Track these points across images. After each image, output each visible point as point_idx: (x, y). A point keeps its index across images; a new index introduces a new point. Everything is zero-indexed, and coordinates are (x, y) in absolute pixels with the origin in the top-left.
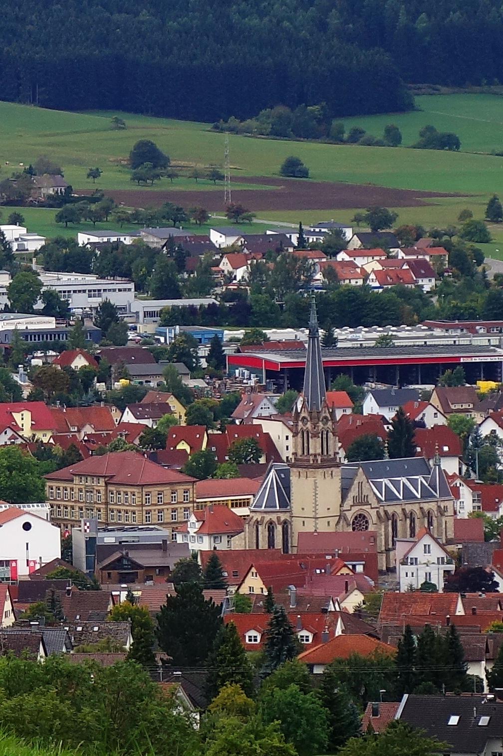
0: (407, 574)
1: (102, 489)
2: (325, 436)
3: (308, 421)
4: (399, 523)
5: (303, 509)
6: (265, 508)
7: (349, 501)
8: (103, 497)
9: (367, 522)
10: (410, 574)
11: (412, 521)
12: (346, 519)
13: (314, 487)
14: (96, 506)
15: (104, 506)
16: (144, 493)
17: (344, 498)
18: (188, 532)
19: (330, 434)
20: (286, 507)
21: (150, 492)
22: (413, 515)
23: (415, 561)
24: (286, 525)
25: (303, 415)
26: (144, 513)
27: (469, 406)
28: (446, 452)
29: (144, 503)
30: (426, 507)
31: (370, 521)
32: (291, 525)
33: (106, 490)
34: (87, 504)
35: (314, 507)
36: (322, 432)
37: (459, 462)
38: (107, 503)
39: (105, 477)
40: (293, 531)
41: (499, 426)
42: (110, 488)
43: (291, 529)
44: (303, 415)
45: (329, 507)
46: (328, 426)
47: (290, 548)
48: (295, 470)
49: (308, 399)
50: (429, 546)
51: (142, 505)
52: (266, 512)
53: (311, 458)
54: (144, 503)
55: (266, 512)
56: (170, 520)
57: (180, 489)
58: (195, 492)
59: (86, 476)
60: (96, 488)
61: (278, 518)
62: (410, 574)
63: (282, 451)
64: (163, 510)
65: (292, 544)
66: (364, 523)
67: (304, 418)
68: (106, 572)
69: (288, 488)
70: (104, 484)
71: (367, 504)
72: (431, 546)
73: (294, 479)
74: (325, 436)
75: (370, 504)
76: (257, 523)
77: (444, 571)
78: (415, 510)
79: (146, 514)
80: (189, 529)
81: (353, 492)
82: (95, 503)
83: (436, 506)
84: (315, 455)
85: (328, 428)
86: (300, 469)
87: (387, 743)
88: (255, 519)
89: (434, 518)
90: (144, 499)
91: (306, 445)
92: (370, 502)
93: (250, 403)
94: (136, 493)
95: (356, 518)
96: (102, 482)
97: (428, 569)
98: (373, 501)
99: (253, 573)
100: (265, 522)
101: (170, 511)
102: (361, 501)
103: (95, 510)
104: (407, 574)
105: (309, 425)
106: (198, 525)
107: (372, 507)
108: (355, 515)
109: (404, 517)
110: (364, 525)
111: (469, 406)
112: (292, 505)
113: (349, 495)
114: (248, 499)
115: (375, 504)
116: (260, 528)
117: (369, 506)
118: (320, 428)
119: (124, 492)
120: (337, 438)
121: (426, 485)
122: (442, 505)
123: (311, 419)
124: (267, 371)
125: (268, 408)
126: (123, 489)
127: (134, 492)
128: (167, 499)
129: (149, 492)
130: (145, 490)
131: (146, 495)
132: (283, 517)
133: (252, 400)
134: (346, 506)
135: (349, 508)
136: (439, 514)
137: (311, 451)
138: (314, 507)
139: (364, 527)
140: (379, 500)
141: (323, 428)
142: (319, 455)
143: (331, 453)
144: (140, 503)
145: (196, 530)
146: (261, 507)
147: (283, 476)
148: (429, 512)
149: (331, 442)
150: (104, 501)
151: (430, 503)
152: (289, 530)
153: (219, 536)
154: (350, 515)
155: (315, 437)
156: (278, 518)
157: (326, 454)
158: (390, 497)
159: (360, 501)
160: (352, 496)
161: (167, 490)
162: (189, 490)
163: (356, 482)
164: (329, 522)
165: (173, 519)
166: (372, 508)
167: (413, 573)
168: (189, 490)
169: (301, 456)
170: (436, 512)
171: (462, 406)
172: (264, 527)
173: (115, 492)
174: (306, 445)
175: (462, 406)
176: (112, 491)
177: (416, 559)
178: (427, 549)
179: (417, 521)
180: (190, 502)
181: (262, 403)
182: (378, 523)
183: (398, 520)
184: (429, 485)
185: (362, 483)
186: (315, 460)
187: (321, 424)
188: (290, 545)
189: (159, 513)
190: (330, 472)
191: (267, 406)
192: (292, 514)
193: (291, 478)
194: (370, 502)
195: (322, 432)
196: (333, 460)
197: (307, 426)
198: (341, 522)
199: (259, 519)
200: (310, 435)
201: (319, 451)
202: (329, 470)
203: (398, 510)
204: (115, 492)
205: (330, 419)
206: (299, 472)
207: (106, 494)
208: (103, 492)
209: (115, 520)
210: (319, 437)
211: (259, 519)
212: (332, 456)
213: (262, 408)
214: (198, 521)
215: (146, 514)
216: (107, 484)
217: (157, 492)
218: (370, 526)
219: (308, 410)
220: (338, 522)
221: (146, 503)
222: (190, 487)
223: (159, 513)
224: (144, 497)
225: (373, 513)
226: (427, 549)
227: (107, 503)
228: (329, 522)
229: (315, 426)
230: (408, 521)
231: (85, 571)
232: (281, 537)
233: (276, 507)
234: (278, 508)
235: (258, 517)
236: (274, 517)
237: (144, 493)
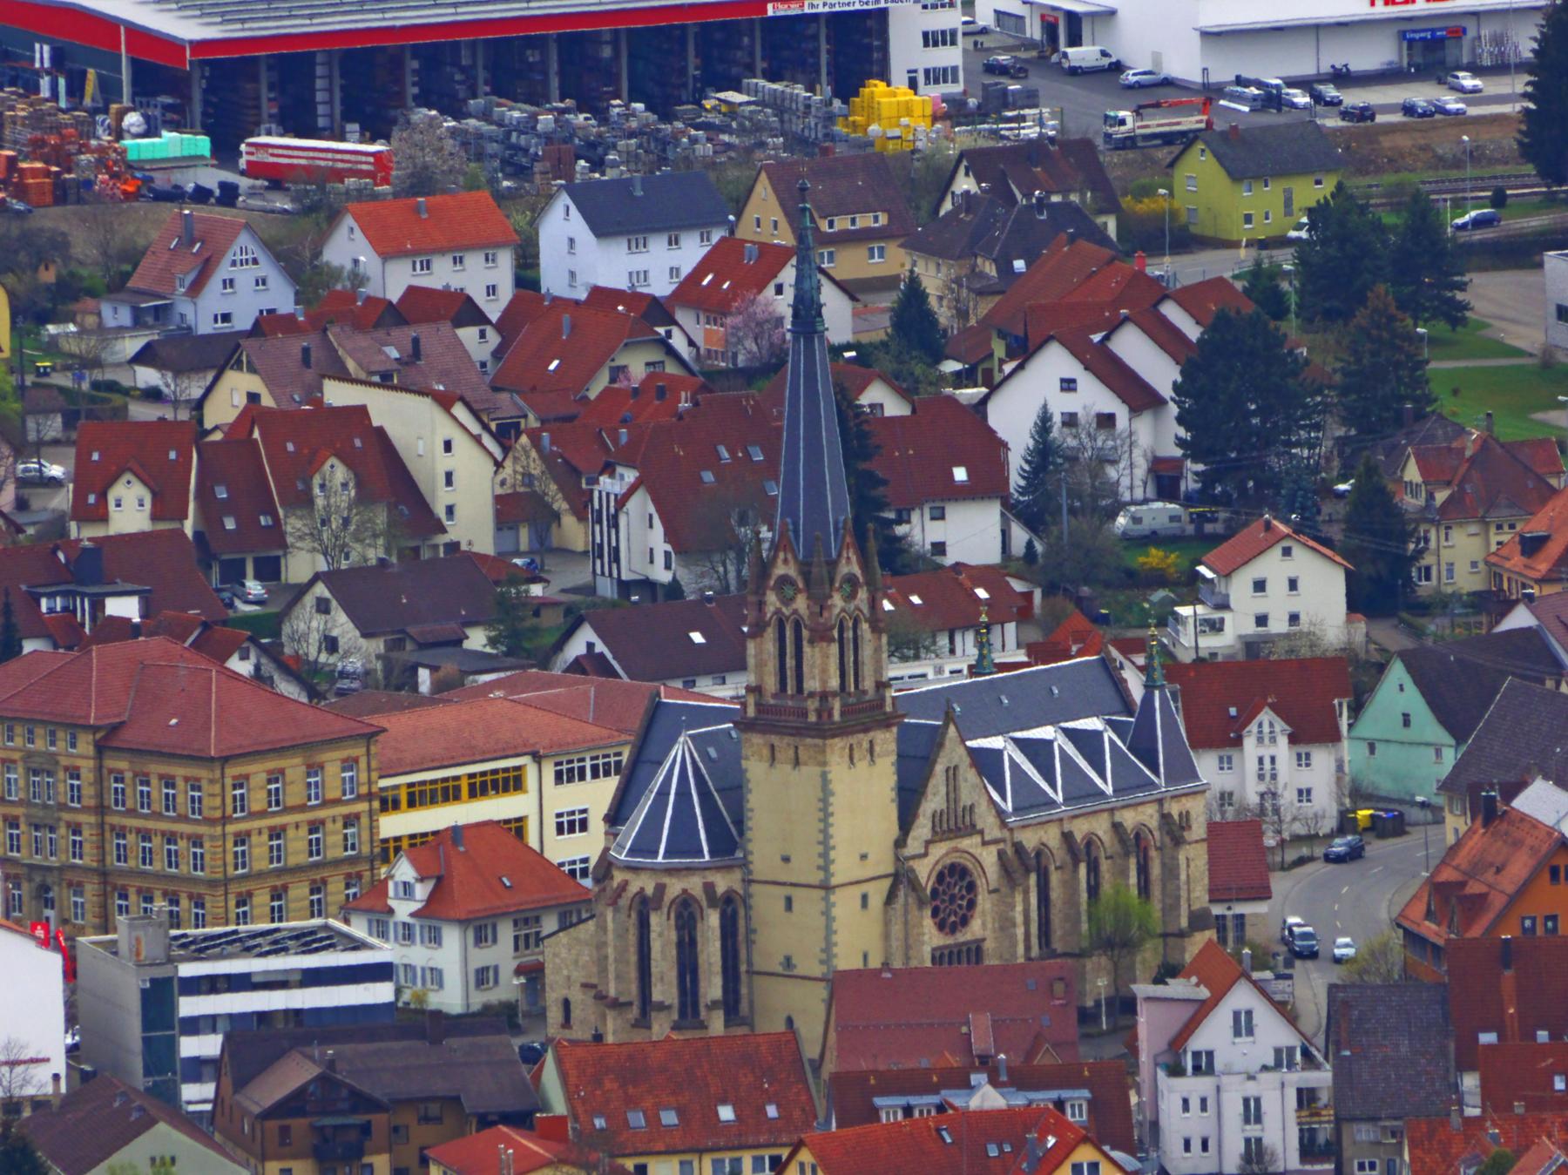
0: (1186, 1102)
1: (87, 767)
2: (849, 634)
3: (797, 591)
4: (1055, 878)
5: (786, 859)
6: (664, 857)
7: (922, 829)
8: (89, 791)
9: (971, 887)
10: (1195, 1104)
11: (1094, 868)
12: (914, 884)
13: (821, 795)
14: (66, 816)
15: (92, 819)
16: (229, 782)
17: (906, 819)
18: (391, 911)
19: (865, 626)
20: (732, 852)
21: (247, 777)
22: (1093, 848)
23: (1204, 1065)
24: (732, 908)
25: (780, 570)
26: (230, 844)
27: (876, 219)
28: (962, 485)
29: (229, 809)
30: (1129, 819)
31: (981, 883)
32: (748, 907)
33: (99, 768)
34: (33, 811)
35: (820, 855)
36: (841, 622)
37: (1002, 514)
38: (101, 809)
39: (95, 729)
40: (754, 925)
41: (1086, 369)
42: (110, 763)
43: (748, 918)
44: (780, 570)
45: (864, 850)
46: (857, 602)
47: (744, 977)
48: (757, 739)
49: (796, 524)
50: (1249, 1013)
51: (225, 820)
52: (670, 871)
53: (812, 705)
54: (229, 809)
55: (670, 871)
56: (303, 859)
57: (332, 760)
58: (374, 764)
59: (31, 723)
60: (64, 761)
61: (709, 888)
62: (1195, 1104)
63: (434, 491)
64: (284, 828)
65: (750, 963)
66: (964, 892)
67: (784, 580)
68: (273, 1125)
69: (735, 791)
70: (91, 751)
71: (972, 830)
72: (1255, 1015)
73: (755, 769)
74: (849, 634)
75: (981, 832)
76: (644, 906)
77: (1300, 1091)
78: (1100, 833)
79: (236, 844)
80: (392, 903)
81: (934, 801)
82: (63, 807)
83: (1156, 816)
84: (824, 696)
85: (858, 608)
86: (775, 739)
87: (124, 1094)
88: (633, 888)
89: (1153, 853)
90: (229, 800)
91: (790, 662)
92: (978, 827)
93: (193, 244)
94: (204, 784)
95: (940, 877)
96: (85, 745)
97: (1251, 1089)
98: (986, 821)
99: (802, 1165)
100: (667, 899)
101: (304, 831)
102: (956, 824)
103: (62, 831)
104: (1186, 1102)
105: (801, 603)
106: (422, 891)
107: (987, 838)
108: (939, 867)
109: (1068, 859)
110: (962, 898)
111: (876, 219)
112: (750, 847)
113: (921, 810)
114: (518, 768)
115: (992, 829)
116: (656, 920)
117: (977, 839)
118: (836, 611)
119: (161, 777)
120: (884, 639)
121: (1124, 748)
122: (1174, 809)
123: (807, 582)
124: (136, 65)
125: (255, 261)
126: (156, 768)
127: (198, 780)
128: (294, 796)
129: (241, 776)
130: (232, 771)
131: (235, 787)
132: (722, 883)
133: (196, 234)
134: (914, 845)
135: (922, 851)
136: (1167, 840)
137: (812, 684)
138: (820, 855)
139: (964, 903)
140: (1001, 813)
141: (843, 610)
142: (834, 694)
143: (868, 684)
144: (218, 814)
145: (418, 906)
146: (655, 854)
147: (712, 752)
148: (1137, 836)
149: (867, 652)
150: (92, 803)
151: (1140, 809)
152: (741, 923)
153: (489, 922)
154: (924, 871)
155: (822, 639)
156: (709, 888)
157: (852, 689)
158: (1031, 801)
159: (952, 823)
160: (929, 813)
161: (294, 767)
162: (356, 760)
163: (939, 768)
164: (865, 898)
165: (311, 854)
166: (985, 843)
167: (1204, 1101)
168: (356, 760)
169: (775, 696)
170: (1157, 834)
171: (853, 221)
172: (665, 917)
173: (128, 775)
174: (790, 662)
175: (853, 221)
176: (121, 772)
177: (1210, 1054)
178: (1243, 1025)
179: (1105, 866)
180: (360, 798)
181: (236, 248)
182: (1004, 890)
183: (1052, 868)
184: (1129, 749)
185: (956, 768)
186: (824, 711)
187: (837, 601)
188: (743, 968)
189: (271, 839)
190: (866, 745)
191: (250, 256)
192: (750, 872)
193: (744, 763)
194: (979, 827)
195: (841, 622)
196: (872, 708)
197: (794, 606)
198: (901, 893)
199: (650, 890)
200: (805, 633)
201: (834, 683)
202: (864, 739)
203: (1052, 837)
204: (128, 775)
205: (861, 579)
206: (772, 747)
207: (99, 780)
208: (87, 775)
209: (132, 863)
210: (832, 640)
211: (650, 890)
212: (871, 694)
213: (234, 263)
214: (421, 880)
215: (236, 844)
216: (101, 749)
217: (264, 776)
218: (980, 898)
219: (795, 557)
220: (890, 898)
221: (235, 811)
222: (359, 751)
223: (271, 839)
224: (230, 793)
225: (989, 857)
226: (1243, 1025)
227: (101, 809)
228: (865, 898)
229: (820, 603)
230: (1083, 870)
231: (140, 1081)
232: (718, 944)
233: (700, 853)
234: (707, 858)
235: (647, 884)
236: (694, 884)
237: (229, 782)
